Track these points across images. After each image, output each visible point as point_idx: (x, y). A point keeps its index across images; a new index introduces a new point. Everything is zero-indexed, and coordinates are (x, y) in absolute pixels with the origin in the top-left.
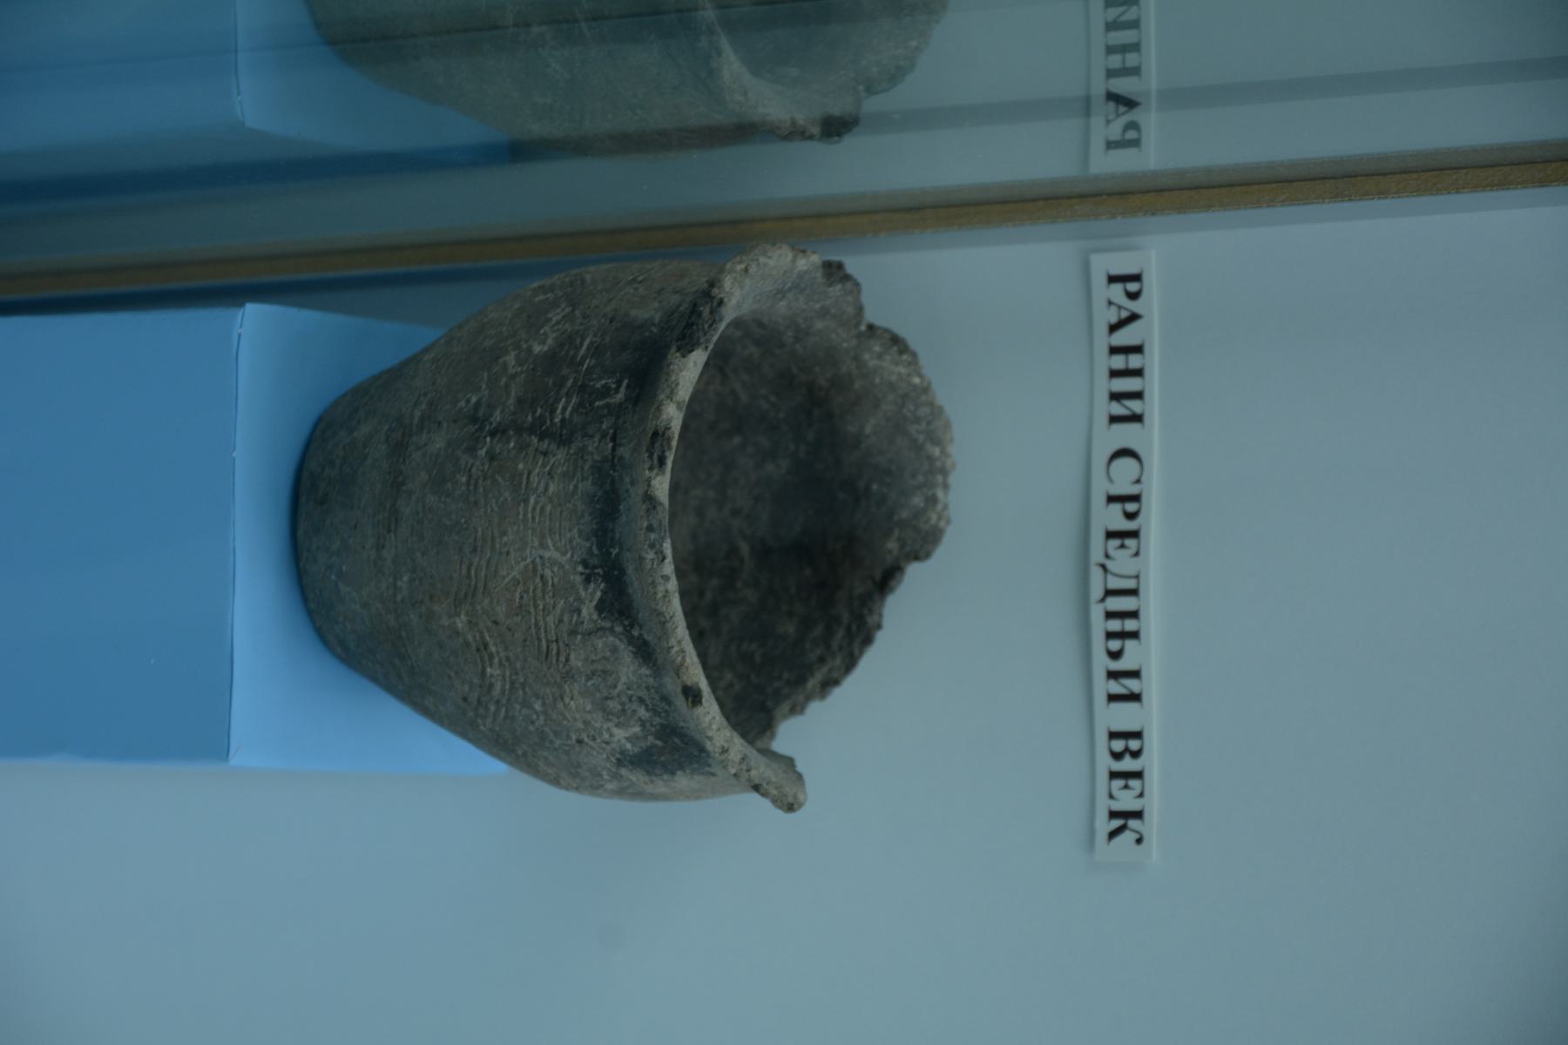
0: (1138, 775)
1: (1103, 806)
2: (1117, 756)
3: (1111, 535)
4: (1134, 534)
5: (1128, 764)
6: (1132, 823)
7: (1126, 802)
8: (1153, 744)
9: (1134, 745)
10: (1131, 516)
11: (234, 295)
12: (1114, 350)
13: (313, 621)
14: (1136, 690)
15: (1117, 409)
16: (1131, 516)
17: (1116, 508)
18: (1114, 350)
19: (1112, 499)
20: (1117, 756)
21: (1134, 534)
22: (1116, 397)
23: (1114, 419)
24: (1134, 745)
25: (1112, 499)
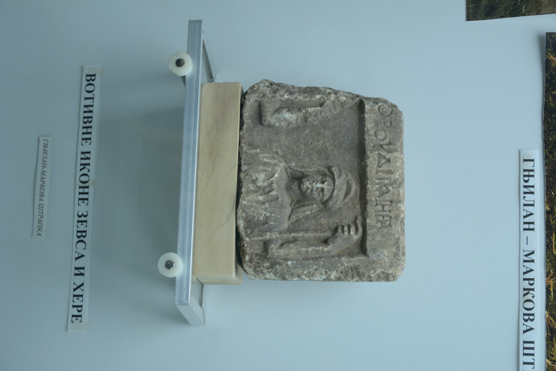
0: (86, 221)
1: (76, 229)
2: (85, 123)
3: (73, 316)
4: (80, 316)
5: (88, 125)
6: (87, 167)
7: (82, 228)
8: (89, 234)
9: (84, 234)
10: (79, 311)
11: (364, 139)
12: (525, 223)
13: (547, 249)
14: (83, 272)
15: (88, 155)
16: (79, 311)
17: (76, 309)
18: (525, 223)
19: (74, 306)
20: (85, 123)
21: (80, 316)
22: (91, 112)
23: (89, 153)
24: (84, 234)
25: (74, 306)
